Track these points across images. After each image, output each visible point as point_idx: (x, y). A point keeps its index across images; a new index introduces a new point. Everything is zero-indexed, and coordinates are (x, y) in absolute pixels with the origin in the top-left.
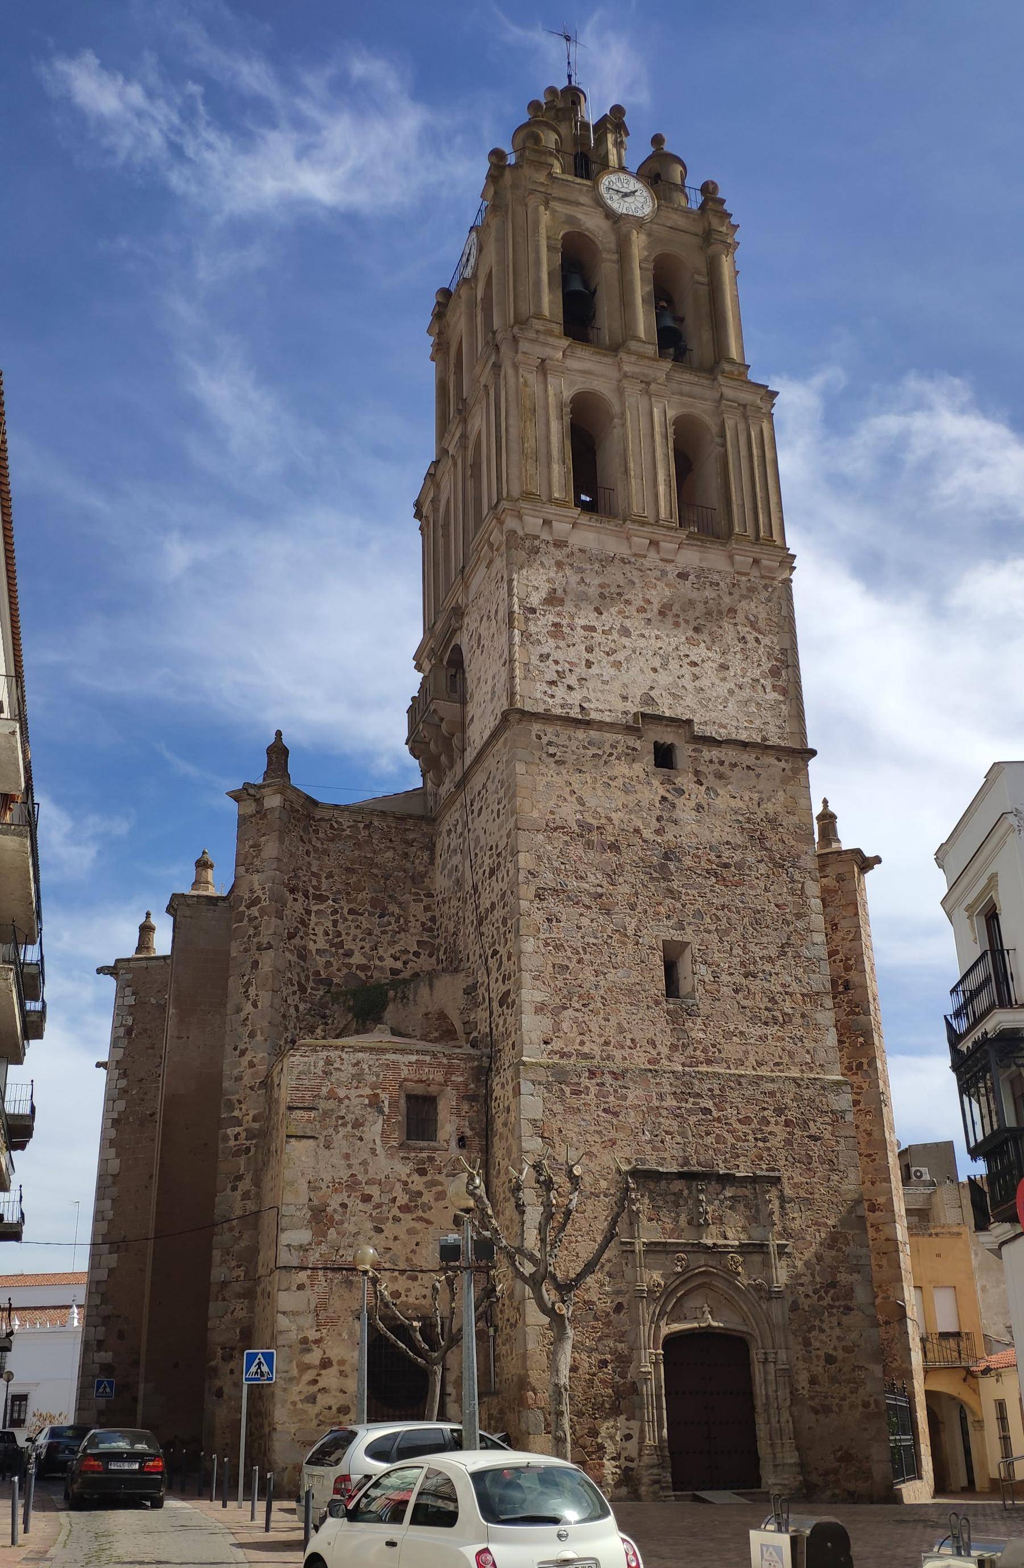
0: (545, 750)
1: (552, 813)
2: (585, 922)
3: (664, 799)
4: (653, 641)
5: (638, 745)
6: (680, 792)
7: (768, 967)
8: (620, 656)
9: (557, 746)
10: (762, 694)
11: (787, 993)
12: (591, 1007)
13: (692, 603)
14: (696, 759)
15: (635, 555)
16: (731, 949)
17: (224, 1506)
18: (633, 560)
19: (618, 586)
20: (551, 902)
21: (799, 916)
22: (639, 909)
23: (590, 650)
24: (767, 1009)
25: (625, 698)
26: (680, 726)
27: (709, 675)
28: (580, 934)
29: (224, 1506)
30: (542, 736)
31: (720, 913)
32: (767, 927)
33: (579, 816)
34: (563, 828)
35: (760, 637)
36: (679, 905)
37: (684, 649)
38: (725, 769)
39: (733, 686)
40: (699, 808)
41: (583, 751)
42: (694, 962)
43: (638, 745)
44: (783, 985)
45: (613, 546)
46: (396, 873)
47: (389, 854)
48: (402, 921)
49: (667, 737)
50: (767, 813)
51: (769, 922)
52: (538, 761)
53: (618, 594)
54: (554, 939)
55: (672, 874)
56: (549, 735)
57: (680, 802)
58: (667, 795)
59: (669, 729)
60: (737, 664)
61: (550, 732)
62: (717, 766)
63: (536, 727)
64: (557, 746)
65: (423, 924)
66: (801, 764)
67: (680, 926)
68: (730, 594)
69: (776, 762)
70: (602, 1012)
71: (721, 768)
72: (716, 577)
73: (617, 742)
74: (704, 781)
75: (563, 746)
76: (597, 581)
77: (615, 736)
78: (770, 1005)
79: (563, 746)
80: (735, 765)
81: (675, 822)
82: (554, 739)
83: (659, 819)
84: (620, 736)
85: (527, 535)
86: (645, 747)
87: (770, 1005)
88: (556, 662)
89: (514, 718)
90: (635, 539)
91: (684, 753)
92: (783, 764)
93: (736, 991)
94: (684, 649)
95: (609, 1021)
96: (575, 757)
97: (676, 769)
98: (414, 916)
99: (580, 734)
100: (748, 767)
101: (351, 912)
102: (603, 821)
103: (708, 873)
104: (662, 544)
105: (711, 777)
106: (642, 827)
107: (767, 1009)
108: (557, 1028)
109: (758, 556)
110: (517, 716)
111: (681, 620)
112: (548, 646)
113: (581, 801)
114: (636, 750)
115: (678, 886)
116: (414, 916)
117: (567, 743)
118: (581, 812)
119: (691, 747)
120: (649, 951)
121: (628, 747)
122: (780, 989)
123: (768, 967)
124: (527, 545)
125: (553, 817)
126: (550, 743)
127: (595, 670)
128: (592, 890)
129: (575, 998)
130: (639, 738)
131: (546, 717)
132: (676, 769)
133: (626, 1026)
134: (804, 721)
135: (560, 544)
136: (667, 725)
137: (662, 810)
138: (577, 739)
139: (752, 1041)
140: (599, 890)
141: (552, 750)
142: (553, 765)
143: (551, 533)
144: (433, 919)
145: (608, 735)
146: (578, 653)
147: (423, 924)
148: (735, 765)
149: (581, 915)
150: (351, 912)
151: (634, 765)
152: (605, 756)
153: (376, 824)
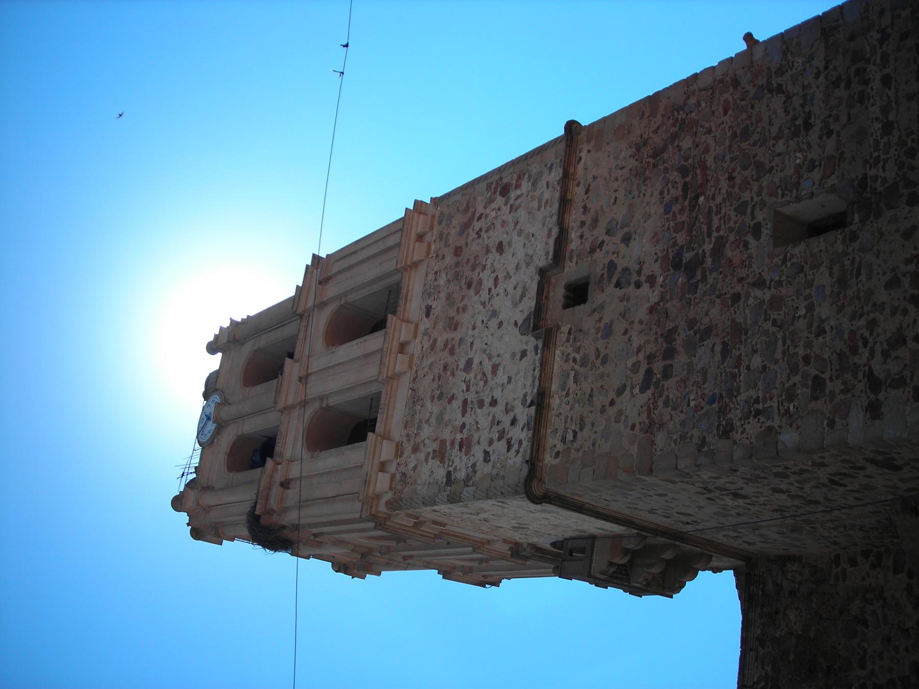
0: (569, 445)
1: (633, 427)
2: (757, 361)
3: (618, 285)
4: (476, 331)
5: (565, 329)
6: (612, 266)
7: (797, 101)
8: (488, 366)
9: (566, 429)
10: (523, 198)
11: (826, 68)
12: (867, 334)
13: (449, 297)
14: (579, 256)
15: (410, 367)
16: (780, 154)
17: (748, 38)
18: (415, 368)
19: (433, 380)
20: (735, 415)
21: (736, 83)
22: (738, 288)
23: (481, 404)
24: (848, 87)
25: (524, 354)
26: (549, 283)
27: (508, 261)
28: (773, 367)
29: (748, 38)
30: (556, 450)
31: (738, 181)
32: (750, 117)
33: (636, 391)
34: (649, 409)
35: (477, 215)
36: (732, 238)
37: (484, 295)
38: (588, 219)
39: (516, 232)
40: (627, 239)
41: (571, 396)
42: (798, 199)
43: (565, 329)
44: (817, 76)
45: (402, 393)
46: (814, 605)
47: (792, 615)
48: (870, 596)
49: (558, 293)
50: (630, 156)
51: (744, 116)
52: (580, 453)
53: (439, 379)
54: (780, 404)
55: (697, 254)
56: (556, 442)
57: (621, 264)
58: (614, 281)
59: (552, 294)
60: (497, 235)
61: (553, 441)
62: (586, 229)
63: (548, 459)
64: (566, 429)
65: (873, 567)
66: (583, 134)
67: (756, 231)
68: (443, 257)
69: (583, 161)
70: (872, 316)
71: (588, 223)
72: (431, 277)
73: (563, 354)
74: (600, 240)
75: (566, 422)
76: (428, 404)
77: (557, 359)
78: (843, 85)
79: (566, 422)
80: (585, 208)
81: (641, 263)
82: (559, 435)
83: (638, 285)
84: (558, 352)
85: (391, 488)
86: (565, 320)
87: (843, 85)
88: (491, 442)
89: (537, 489)
90: (397, 369)
91: (572, 271)
92: (584, 154)
93: (830, 133)
94: (484, 295)
95: (883, 303)
96: (577, 405)
97: (589, 277)
98: (863, 579)
99: (555, 402)
100: (587, 191)
101: (862, 666)
102: (641, 355)
103: (694, 207)
104: (402, 339)
105: (596, 233)
106: (648, 305)
107: (848, 87)
108: (898, 382)
109: (413, 236)
110: (535, 484)
111: (461, 305)
112: (478, 453)
113: (620, 391)
114: (570, 329)
115: (710, 243)
116: (863, 579)
117: (563, 417)
118: (633, 387)
119: (568, 264)
120: (789, 264)
121: (568, 341)
122: (822, 78)
123: (797, 101)
124: (399, 487)
125: (638, 427)
126: (564, 440)
127: (497, 394)
128: (718, 357)
129: (856, 359)
130: (558, 327)
131: (537, 444)
132: (589, 277)
133: (888, 276)
134: (544, 145)
135: (399, 451)
136: (547, 298)
137: (629, 284)
138: (559, 406)
139: (891, 93)
140: (718, 348)
141: (570, 437)
142: (584, 432)
143: (390, 461)
144: (866, 554)
145: (556, 367)
146: (482, 417)
147: (873, 567)
148: (585, 208)
149: (748, 368)
150: (862, 666)
151: (585, 329)
152: (576, 367)
153: (759, 632)
